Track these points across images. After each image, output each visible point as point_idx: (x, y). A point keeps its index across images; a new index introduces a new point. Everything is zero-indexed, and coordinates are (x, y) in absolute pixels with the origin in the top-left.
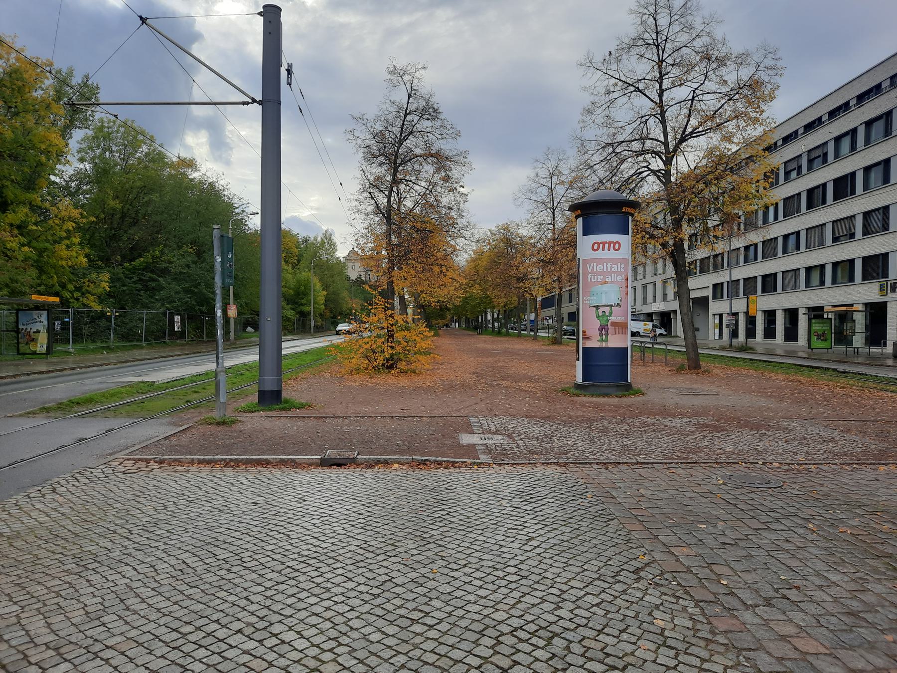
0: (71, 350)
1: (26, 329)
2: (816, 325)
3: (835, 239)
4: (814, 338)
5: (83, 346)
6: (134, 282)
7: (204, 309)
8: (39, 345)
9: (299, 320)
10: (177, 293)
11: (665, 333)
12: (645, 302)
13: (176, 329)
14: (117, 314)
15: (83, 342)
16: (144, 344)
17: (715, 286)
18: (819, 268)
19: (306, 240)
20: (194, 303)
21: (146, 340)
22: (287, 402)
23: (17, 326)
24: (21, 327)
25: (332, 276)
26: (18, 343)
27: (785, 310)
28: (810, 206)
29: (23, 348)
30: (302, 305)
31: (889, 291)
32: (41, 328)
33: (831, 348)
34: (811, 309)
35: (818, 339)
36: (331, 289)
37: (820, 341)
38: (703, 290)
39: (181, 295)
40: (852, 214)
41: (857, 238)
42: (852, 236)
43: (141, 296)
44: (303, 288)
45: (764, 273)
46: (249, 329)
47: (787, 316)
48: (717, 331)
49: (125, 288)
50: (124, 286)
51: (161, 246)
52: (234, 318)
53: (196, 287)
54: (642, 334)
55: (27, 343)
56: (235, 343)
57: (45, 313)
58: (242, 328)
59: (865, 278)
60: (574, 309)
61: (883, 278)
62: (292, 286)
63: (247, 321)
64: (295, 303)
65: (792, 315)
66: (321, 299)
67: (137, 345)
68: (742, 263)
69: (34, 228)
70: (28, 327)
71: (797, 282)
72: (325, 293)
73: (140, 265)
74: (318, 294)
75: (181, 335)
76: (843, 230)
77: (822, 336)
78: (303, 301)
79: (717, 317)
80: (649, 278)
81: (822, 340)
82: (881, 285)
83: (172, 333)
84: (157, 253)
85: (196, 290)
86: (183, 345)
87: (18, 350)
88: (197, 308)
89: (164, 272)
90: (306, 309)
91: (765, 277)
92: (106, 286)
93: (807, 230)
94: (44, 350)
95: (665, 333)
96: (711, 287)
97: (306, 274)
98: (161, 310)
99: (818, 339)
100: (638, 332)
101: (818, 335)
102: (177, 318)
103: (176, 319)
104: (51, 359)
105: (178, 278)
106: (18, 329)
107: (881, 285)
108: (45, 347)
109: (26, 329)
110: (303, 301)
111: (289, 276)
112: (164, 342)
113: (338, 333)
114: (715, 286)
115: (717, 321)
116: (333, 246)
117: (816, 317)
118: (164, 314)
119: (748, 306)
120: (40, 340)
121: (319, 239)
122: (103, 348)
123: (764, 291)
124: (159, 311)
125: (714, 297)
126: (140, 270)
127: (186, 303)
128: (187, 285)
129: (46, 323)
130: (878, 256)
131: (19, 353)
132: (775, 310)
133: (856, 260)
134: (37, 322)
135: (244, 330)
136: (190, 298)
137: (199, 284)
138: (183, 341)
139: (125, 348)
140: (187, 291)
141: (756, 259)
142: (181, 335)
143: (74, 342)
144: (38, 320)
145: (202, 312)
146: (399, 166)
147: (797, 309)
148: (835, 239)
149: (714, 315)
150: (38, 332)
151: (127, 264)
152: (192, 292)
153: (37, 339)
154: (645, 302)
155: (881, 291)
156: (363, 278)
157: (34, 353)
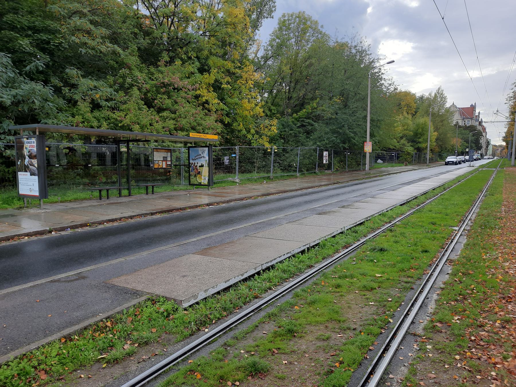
0: (237, 181)
5: (248, 176)
6: (298, 127)
7: (346, 146)
8: (203, 178)
9: (416, 154)
10: (326, 133)
13: (324, 162)
14: (349, 154)
16: (298, 174)
19: (422, 98)
20: (339, 141)
21: (300, 171)
24: (191, 161)
25: (442, 121)
26: (190, 175)
29: (193, 180)
30: (420, 142)
36: (441, 131)
39: (329, 136)
43: (301, 136)
44: (421, 130)
46: (379, 161)
49: (291, 132)
50: (292, 130)
51: (318, 99)
52: (370, 153)
53: (341, 129)
55: (195, 176)
56: (370, 173)
57: (207, 149)
58: (374, 160)
62: (412, 129)
63: (378, 155)
64: (413, 141)
66: (434, 138)
67: (292, 175)
69: (226, 86)
70: (196, 162)
72: (436, 133)
73: (303, 115)
74: (432, 135)
75: (329, 167)
78: (420, 140)
83: (321, 165)
84: (315, 104)
85: (341, 131)
86: (330, 174)
89: (318, 118)
90: (423, 145)
92: (275, 130)
97: (421, 120)
98: (313, 147)
102: (325, 153)
103: (324, 154)
104: (211, 191)
105: (328, 122)
106: (189, 163)
110: (420, 140)
111: (410, 122)
112: (315, 172)
113: (447, 164)
116: (444, 99)
118: (315, 150)
121: (433, 95)
122: (264, 178)
124: (311, 147)
126: (302, 118)
127: (332, 141)
128: (334, 128)
129: (207, 158)
131: (190, 184)
134: (201, 157)
135: (376, 162)
136: (336, 137)
137: (343, 126)
138: (329, 172)
139: (282, 178)
140: (334, 132)
142: (329, 167)
143: (242, 172)
144: (202, 155)
145: (345, 149)
150: (202, 166)
151: (295, 115)
152: (338, 132)
156: (460, 124)
157: (200, 184)
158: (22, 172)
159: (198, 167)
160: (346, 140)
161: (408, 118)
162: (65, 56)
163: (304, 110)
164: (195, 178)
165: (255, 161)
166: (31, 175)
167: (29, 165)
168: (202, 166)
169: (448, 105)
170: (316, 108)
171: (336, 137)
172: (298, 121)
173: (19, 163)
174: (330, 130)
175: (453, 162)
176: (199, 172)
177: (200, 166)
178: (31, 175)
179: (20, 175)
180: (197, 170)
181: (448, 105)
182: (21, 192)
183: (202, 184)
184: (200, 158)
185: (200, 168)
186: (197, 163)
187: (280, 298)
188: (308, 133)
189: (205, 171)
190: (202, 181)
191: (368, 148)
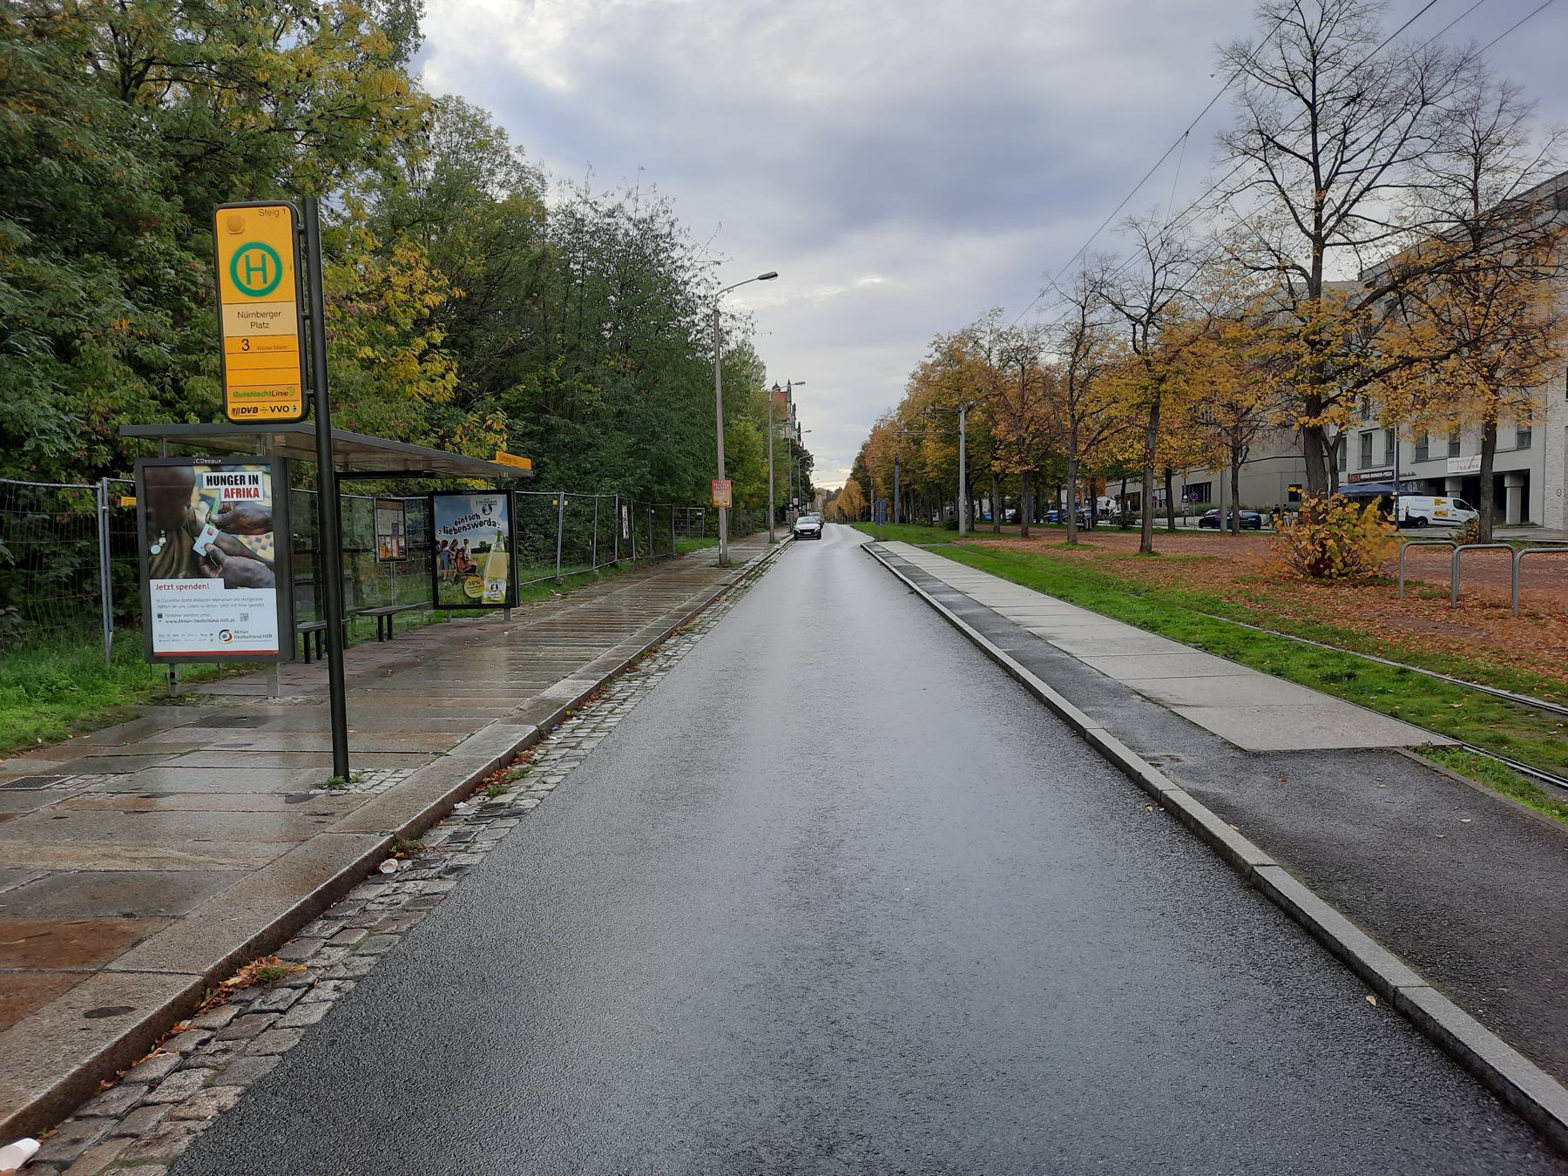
1: (455, 542)
8: (487, 585)
12: (1422, 454)
15: (94, 637)
22: (1533, 524)
23: (431, 533)
29: (447, 592)
32: (491, 540)
54: (1431, 521)
61: (111, 535)
87: (436, 597)
88: (656, 487)
94: (500, 596)
100: (1423, 519)
106: (434, 542)
108: (503, 587)
109: (455, 542)
120: (488, 572)
129: (504, 526)
134: (481, 524)
144: (483, 518)
146: (1483, 248)
150: (485, 549)
153: (483, 568)
154: (1422, 454)
157: (477, 604)
158: (175, 576)
159: (468, 552)
160: (665, 472)
162: (373, 242)
163: (522, 387)
166: (228, 586)
167: (221, 555)
168: (485, 549)
169: (768, 386)
173: (155, 549)
175: (812, 530)
176: (474, 567)
177: (474, 551)
178: (228, 586)
179: (442, 589)
180: (465, 562)
181: (768, 386)
182: (159, 647)
183: (484, 602)
184: (475, 525)
185: (476, 555)
186: (466, 542)
187: (1536, 777)
189: (496, 565)
190: (485, 594)
191: (722, 496)
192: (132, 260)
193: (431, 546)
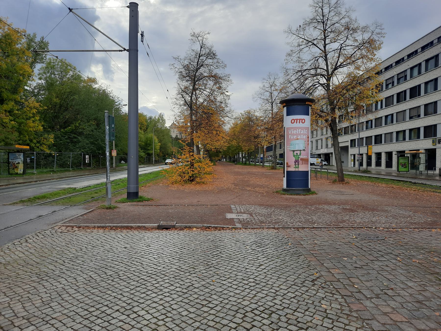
0: (35, 172)
2: (401, 160)
3: (411, 118)
4: (400, 166)
5: (41, 170)
6: (66, 139)
7: (100, 152)
8: (19, 170)
9: (147, 157)
10: (87, 144)
11: (327, 164)
12: (317, 149)
13: (87, 162)
14: (58, 154)
15: (41, 168)
16: (71, 169)
17: (351, 141)
18: (403, 132)
19: (150, 118)
20: (95, 149)
21: (72, 167)
22: (141, 197)
23: (8, 160)
24: (10, 161)
25: (163, 136)
26: (9, 169)
27: (386, 153)
28: (398, 101)
29: (11, 171)
30: (148, 150)
31: (437, 143)
32: (20, 162)
33: (409, 171)
34: (399, 152)
35: (402, 167)
36: (163, 142)
37: (403, 168)
38: (346, 142)
39: (89, 145)
40: (419, 105)
41: (421, 117)
42: (419, 116)
43: (69, 145)
44: (149, 142)
45: (375, 134)
46: (123, 162)
47: (387, 155)
48: (353, 163)
51: (79, 121)
52: (115, 156)
53: (96, 141)
54: (315, 164)
55: (13, 169)
56: (116, 169)
57: (22, 154)
58: (119, 161)
59: (425, 137)
60: (282, 152)
61: (434, 137)
62: (143, 141)
63: (122, 158)
64: (145, 149)
65: (389, 155)
67: (67, 170)
68: (365, 129)
69: (17, 112)
70: (14, 161)
71: (392, 139)
72: (160, 144)
73: (69, 131)
75: (89, 165)
76: (414, 113)
77: (404, 165)
78: (149, 148)
79: (353, 156)
80: (319, 137)
81: (404, 167)
82: (433, 140)
83: (85, 164)
84: (77, 124)
85: (96, 143)
86: (90, 170)
87: (9, 172)
89: (81, 134)
90: (150, 152)
91: (376, 136)
92: (52, 141)
93: (397, 113)
94: (22, 172)
95: (327, 164)
96: (350, 141)
97: (150, 135)
98: (79, 153)
99: (402, 167)
100: (314, 163)
101: (402, 165)
102: (87, 156)
103: (86, 157)
104: (25, 177)
105: (87, 137)
106: (9, 162)
107: (433, 140)
108: (22, 170)
109: (13, 162)
110: (149, 148)
112: (81, 168)
113: (166, 164)
114: (351, 141)
115: (353, 158)
116: (164, 121)
117: (401, 156)
118: (81, 154)
119: (368, 151)
120: (19, 167)
121: (157, 118)
122: (51, 171)
123: (375, 143)
124: (78, 153)
125: (351, 146)
126: (69, 133)
127: (91, 149)
128: (92, 140)
129: (23, 159)
130: (432, 126)
131: (9, 174)
132: (381, 153)
133: (421, 128)
134: (18, 158)
135: (120, 162)
136: (93, 146)
137: (98, 140)
138: (90, 168)
139: (61, 171)
140: (92, 143)
141: (372, 127)
142: (89, 165)
143: (37, 168)
144: (19, 157)
145: (99, 154)
147: (392, 152)
148: (411, 118)
149: (351, 155)
150: (19, 163)
151: (62, 130)
152: (94, 144)
153: (18, 167)
154: (317, 149)
155: (433, 143)
156: (179, 137)
157: (17, 174)
161: (141, 133)
164: (13, 171)
165: (41, 161)
170: (78, 127)
171: (93, 146)
172: (66, 134)
174: (90, 142)
188: (75, 143)
192: (88, 122)
193: (9, 163)
